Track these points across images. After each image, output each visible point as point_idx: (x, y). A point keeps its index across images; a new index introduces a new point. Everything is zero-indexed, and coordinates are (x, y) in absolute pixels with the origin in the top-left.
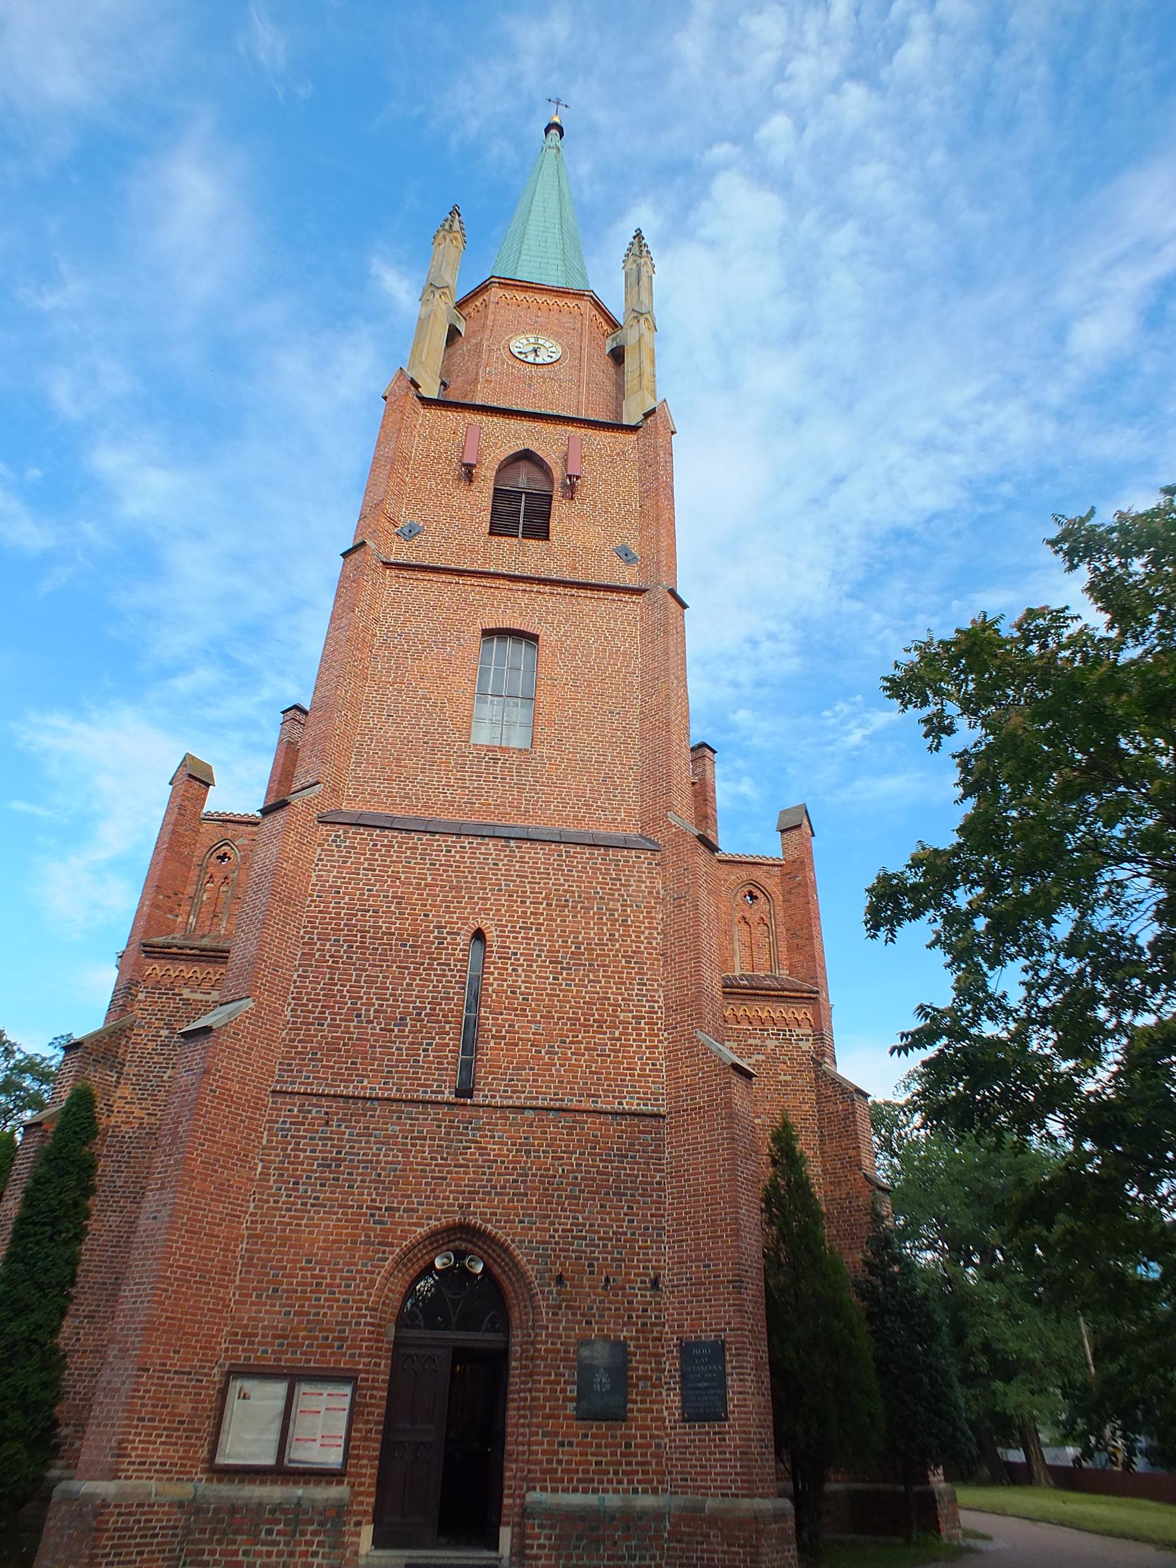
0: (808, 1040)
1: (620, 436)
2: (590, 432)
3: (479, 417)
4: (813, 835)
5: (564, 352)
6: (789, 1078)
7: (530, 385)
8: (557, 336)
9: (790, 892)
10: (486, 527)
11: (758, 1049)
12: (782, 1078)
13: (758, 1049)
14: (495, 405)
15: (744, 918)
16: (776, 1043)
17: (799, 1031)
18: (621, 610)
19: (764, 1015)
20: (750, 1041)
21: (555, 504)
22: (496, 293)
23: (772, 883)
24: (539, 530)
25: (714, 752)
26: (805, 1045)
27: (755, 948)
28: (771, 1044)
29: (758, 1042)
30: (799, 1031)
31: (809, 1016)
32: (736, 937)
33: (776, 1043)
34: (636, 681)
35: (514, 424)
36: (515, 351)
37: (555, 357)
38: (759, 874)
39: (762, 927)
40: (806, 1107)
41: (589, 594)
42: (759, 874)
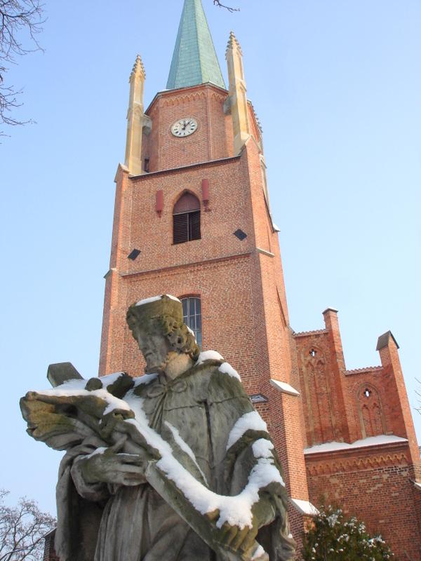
0: (406, 470)
1: (231, 165)
2: (216, 168)
3: (160, 178)
4: (398, 347)
5: (199, 124)
6: (397, 494)
7: (184, 150)
8: (195, 116)
9: (388, 386)
10: (170, 240)
11: (378, 481)
12: (393, 495)
13: (378, 481)
14: (171, 169)
15: (365, 406)
16: (388, 475)
17: (400, 466)
18: (240, 268)
19: (379, 461)
20: (374, 477)
21: (202, 216)
22: (162, 101)
23: (377, 382)
24: (196, 235)
25: (336, 312)
26: (405, 474)
27: (373, 422)
28: (385, 476)
29: (378, 477)
30: (400, 466)
31: (405, 457)
32: (361, 418)
33: (388, 475)
34: (250, 306)
35: (178, 177)
36: (174, 132)
37: (195, 128)
38: (369, 378)
39: (376, 409)
40: (408, 509)
41: (223, 264)
42: (369, 378)
